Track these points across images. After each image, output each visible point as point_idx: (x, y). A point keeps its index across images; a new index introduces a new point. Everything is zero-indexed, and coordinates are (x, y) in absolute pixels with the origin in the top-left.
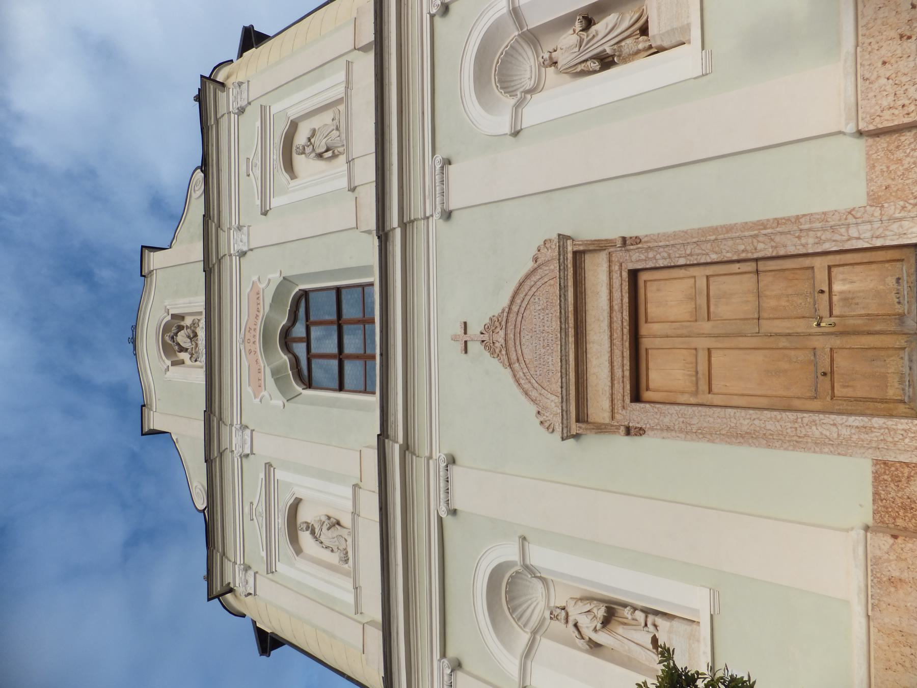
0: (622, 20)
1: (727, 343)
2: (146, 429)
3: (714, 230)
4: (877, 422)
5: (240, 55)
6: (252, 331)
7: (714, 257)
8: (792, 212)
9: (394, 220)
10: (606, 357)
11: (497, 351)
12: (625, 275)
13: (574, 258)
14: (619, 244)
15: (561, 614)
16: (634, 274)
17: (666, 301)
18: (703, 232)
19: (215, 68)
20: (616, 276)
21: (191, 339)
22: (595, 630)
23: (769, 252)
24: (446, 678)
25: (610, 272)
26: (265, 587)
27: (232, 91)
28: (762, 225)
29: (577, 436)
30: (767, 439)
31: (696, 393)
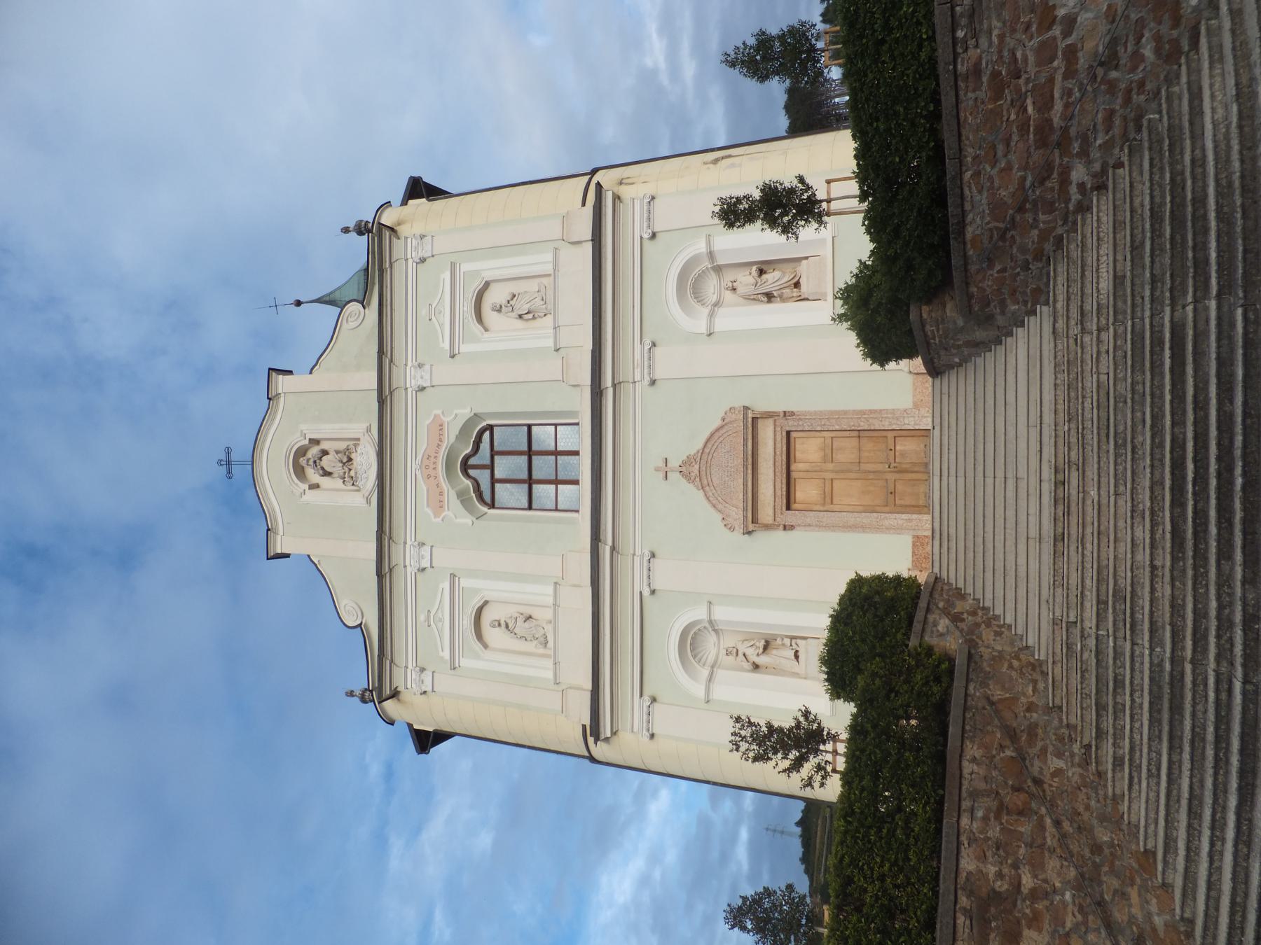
1: (842, 475)
2: (272, 554)
4: (915, 516)
5: (404, 203)
6: (432, 459)
7: (837, 427)
9: (608, 381)
13: (753, 422)
15: (733, 652)
16: (788, 433)
17: (808, 450)
18: (833, 412)
20: (778, 434)
23: (866, 427)
26: (446, 683)
28: (863, 412)
29: (749, 533)
30: (863, 528)
31: (824, 504)
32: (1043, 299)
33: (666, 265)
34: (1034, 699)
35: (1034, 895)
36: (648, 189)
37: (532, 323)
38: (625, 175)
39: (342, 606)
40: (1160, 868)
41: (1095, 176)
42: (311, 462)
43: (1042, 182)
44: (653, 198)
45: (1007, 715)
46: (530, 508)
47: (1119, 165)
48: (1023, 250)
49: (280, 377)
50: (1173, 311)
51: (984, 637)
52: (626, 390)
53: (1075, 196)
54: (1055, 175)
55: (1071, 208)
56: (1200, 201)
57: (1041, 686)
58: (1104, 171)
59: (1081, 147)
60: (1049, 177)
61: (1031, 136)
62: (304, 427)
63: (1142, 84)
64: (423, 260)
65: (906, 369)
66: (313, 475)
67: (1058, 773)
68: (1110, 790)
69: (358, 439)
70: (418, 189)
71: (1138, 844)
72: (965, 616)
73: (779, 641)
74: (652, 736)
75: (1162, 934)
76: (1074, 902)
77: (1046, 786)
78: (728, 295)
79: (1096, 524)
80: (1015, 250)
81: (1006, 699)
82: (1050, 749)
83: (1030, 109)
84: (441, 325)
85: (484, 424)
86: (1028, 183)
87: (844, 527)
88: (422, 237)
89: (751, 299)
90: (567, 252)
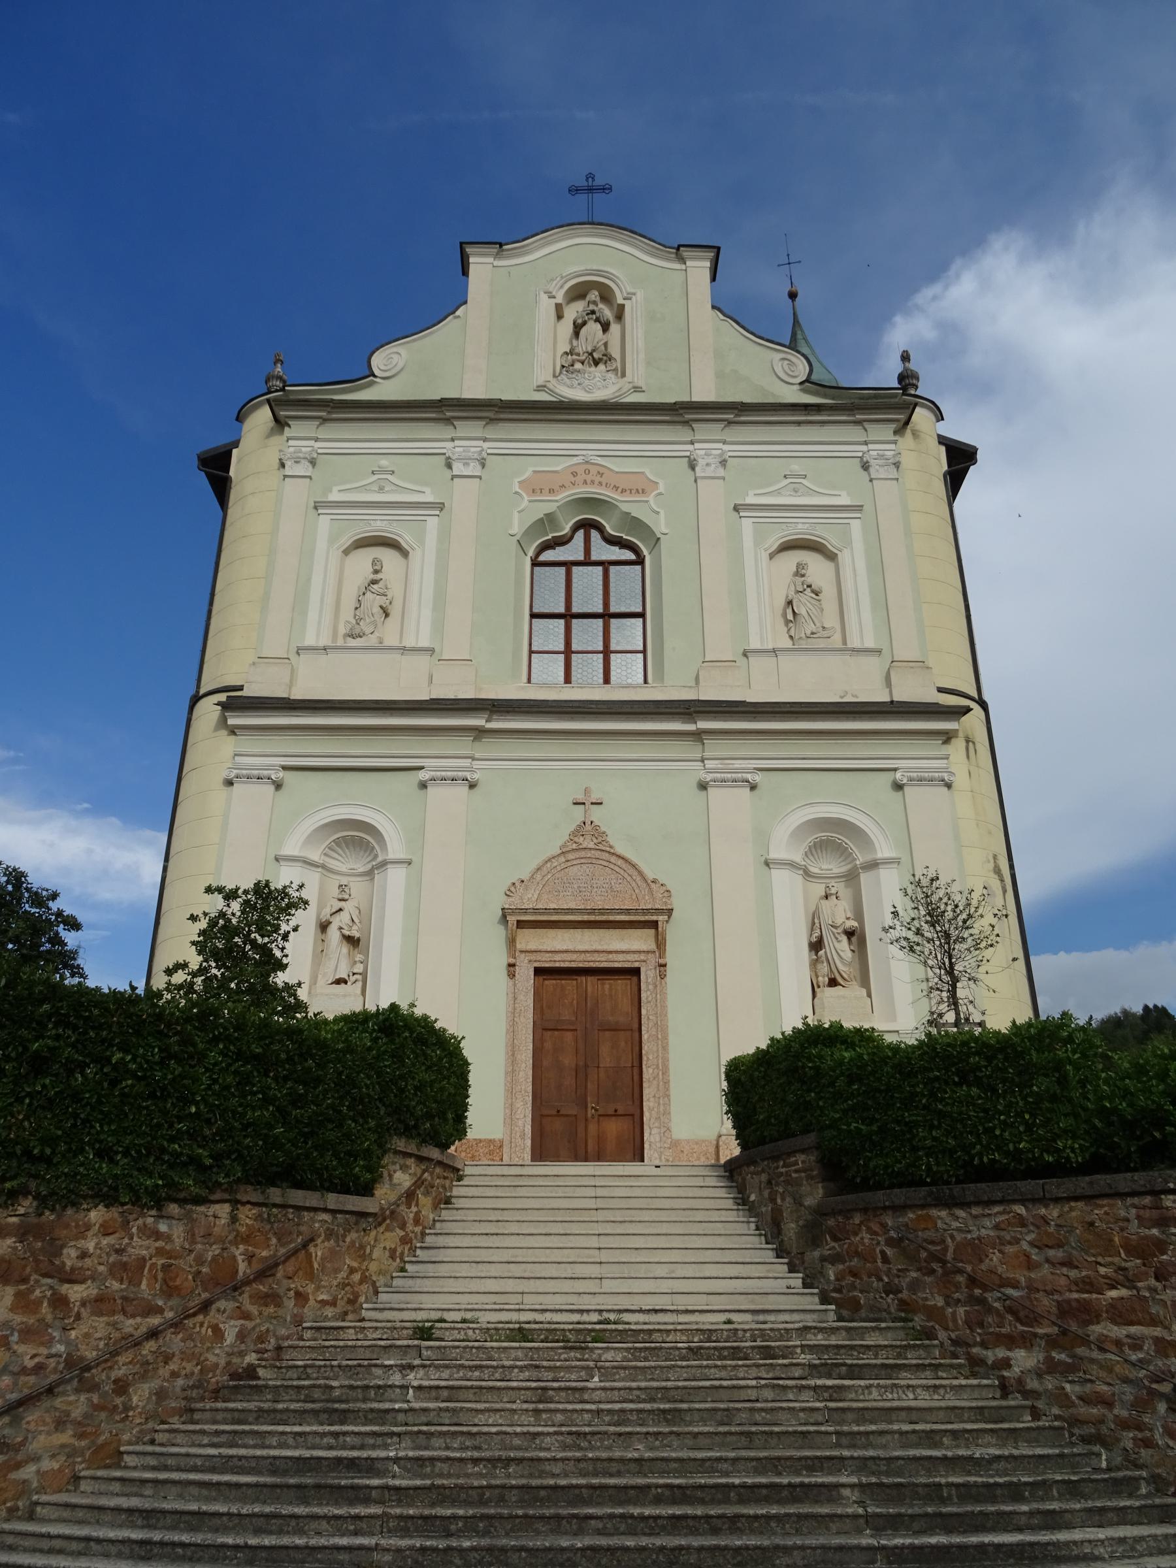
0: (843, 963)
2: (469, 250)
3: (665, 1038)
4: (529, 1143)
5: (942, 440)
6: (598, 479)
8: (673, 1092)
10: (571, 948)
11: (576, 839)
12: (636, 965)
13: (650, 922)
14: (662, 961)
16: (636, 972)
19: (933, 403)
21: (591, 354)
22: (341, 928)
23: (645, 1076)
24: (266, 773)
25: (640, 952)
26: (297, 494)
27: (889, 450)
28: (665, 1071)
32: (845, 1313)
33: (859, 802)
34: (312, 1302)
35: (59, 1302)
36: (961, 780)
37: (780, 621)
38: (978, 746)
39: (401, 350)
40: (100, 1473)
41: (1020, 1381)
42: (592, 307)
43: (1010, 1310)
44: (949, 786)
45: (290, 1267)
46: (534, 616)
47: (1036, 1414)
48: (914, 1286)
49: (708, 264)
50: (852, 1486)
51: (388, 1234)
52: (692, 750)
53: (991, 1355)
54: (1021, 1328)
55: (975, 1350)
56: (1004, 1522)
57: (329, 1312)
58: (1027, 1394)
59: (1060, 1362)
60: (1018, 1320)
61: (1075, 1296)
62: (640, 295)
63: (1148, 1443)
64: (865, 467)
65: (724, 1131)
66: (574, 311)
67: (218, 1333)
68: (200, 1405)
69: (623, 375)
70: (960, 458)
71: (130, 1443)
72: (414, 1209)
73: (359, 957)
74: (229, 783)
75: (13, 1476)
76: (52, 1356)
77: (200, 1317)
78: (820, 889)
79: (556, 1385)
80: (914, 1274)
81: (312, 1267)
82: (249, 1324)
83: (1113, 1294)
84: (778, 492)
85: (645, 552)
86: (1010, 1291)
87: (513, 1046)
88: (897, 465)
89: (814, 921)
90: (874, 667)
